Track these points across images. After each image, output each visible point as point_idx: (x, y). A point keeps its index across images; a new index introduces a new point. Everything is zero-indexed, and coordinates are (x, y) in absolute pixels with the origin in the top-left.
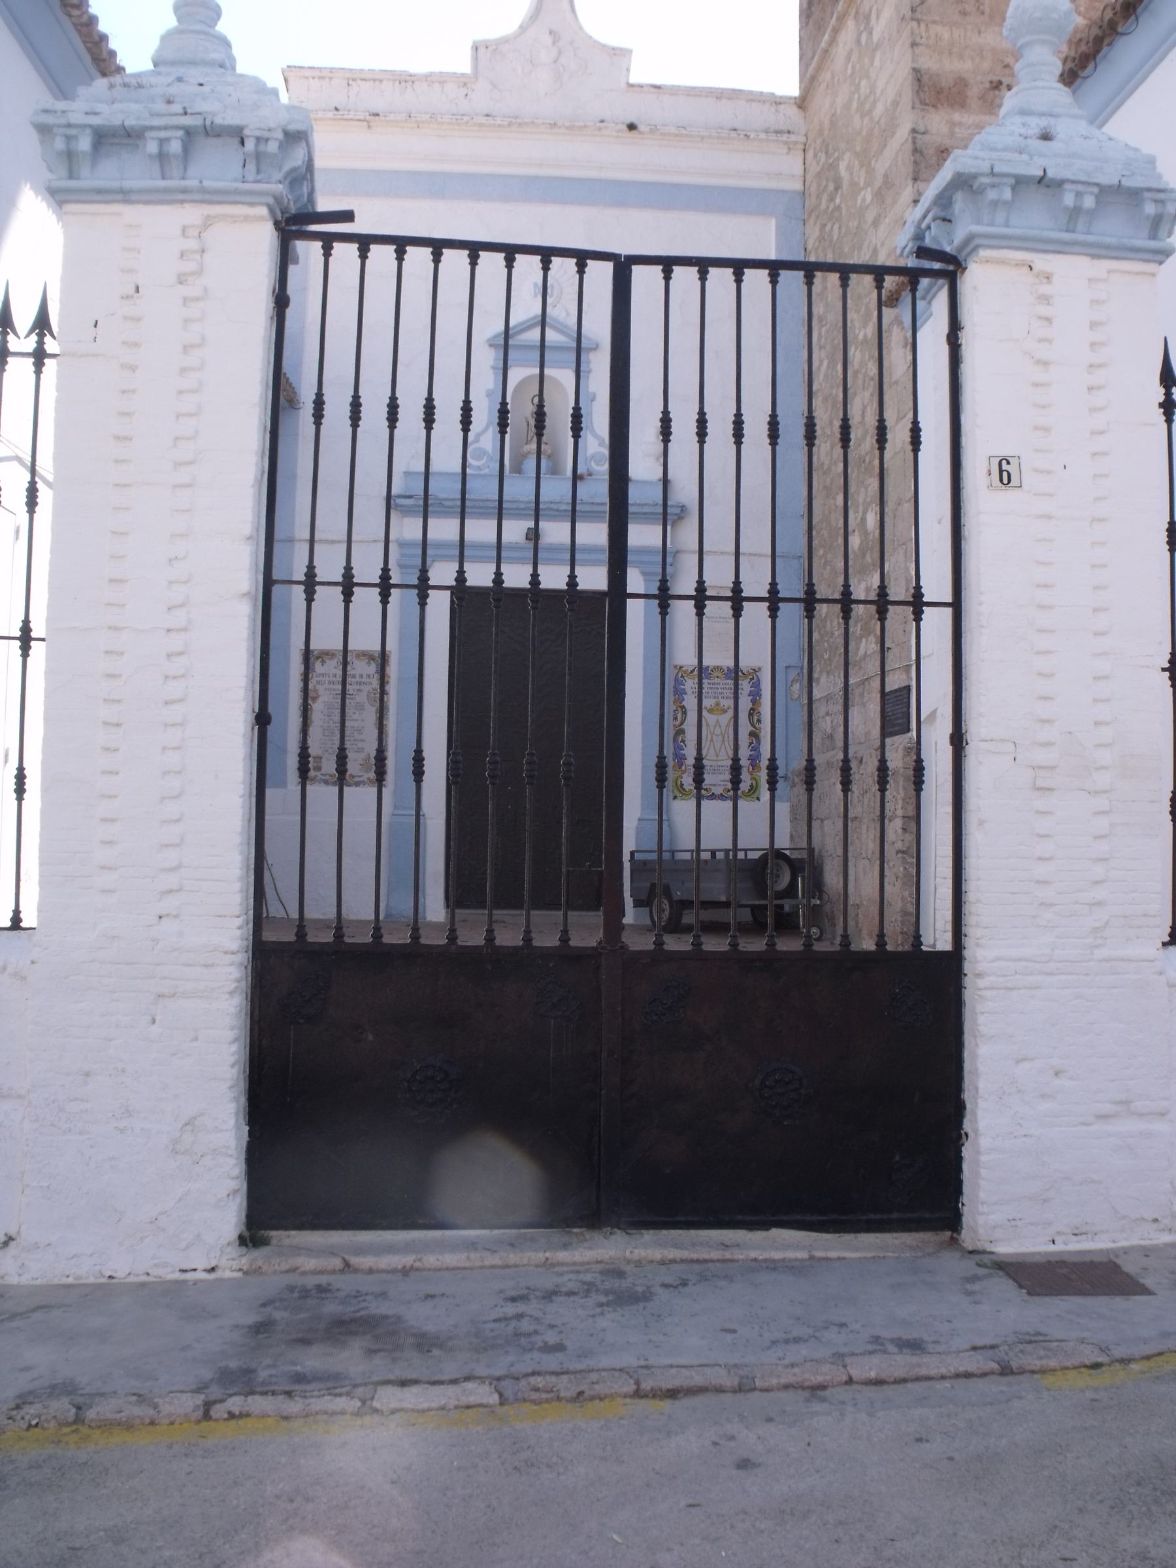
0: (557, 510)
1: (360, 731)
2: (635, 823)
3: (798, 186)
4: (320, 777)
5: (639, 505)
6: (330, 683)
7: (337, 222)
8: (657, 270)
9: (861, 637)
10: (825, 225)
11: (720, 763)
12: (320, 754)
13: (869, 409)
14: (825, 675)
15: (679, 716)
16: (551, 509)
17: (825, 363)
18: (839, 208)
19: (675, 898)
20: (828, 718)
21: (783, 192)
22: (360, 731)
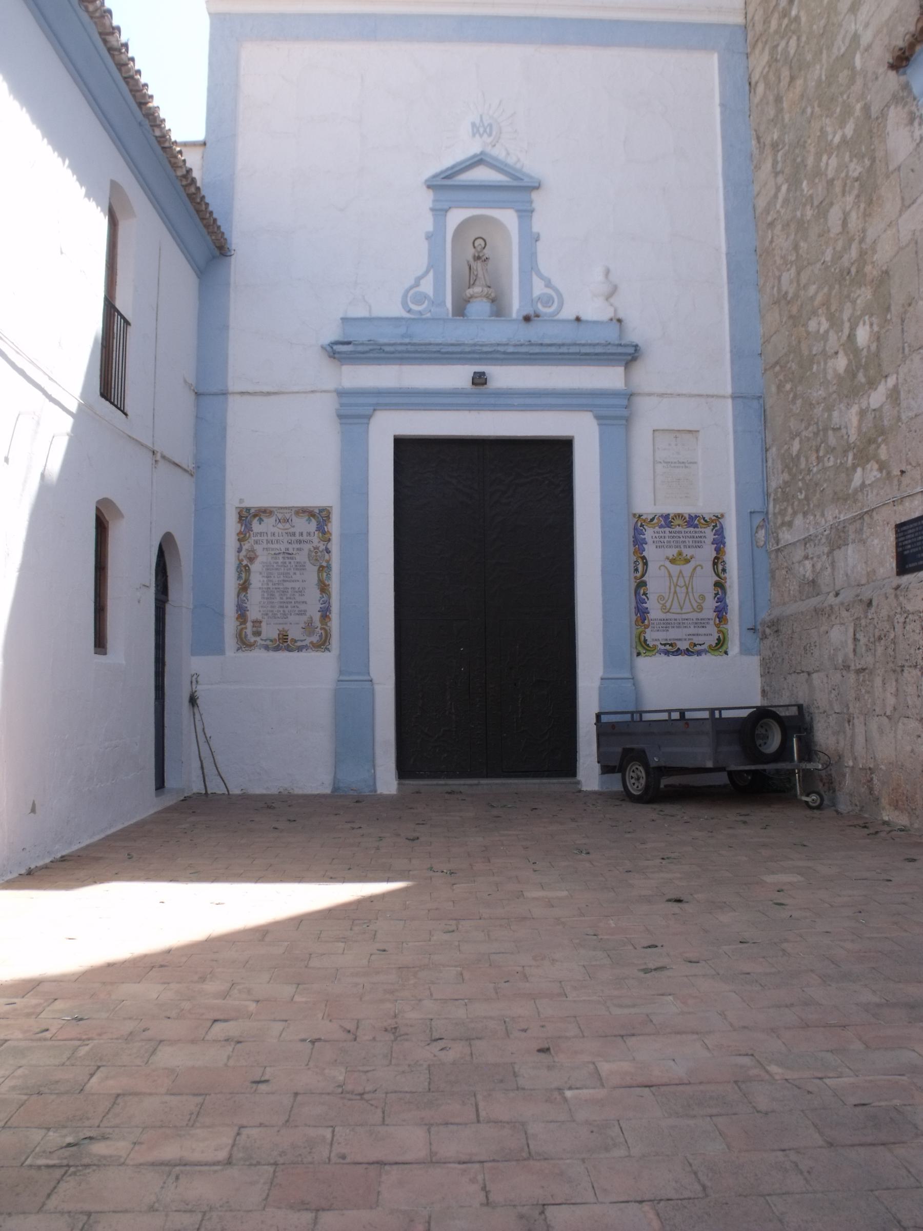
0: (505, 353)
2: (597, 683)
3: (740, 20)
5: (590, 345)
9: (854, 467)
10: (777, 46)
11: (684, 616)
12: (260, 618)
13: (854, 215)
14: (800, 516)
15: (640, 567)
16: (498, 352)
17: (784, 188)
18: (797, 19)
19: (653, 765)
20: (807, 562)
21: (725, 26)
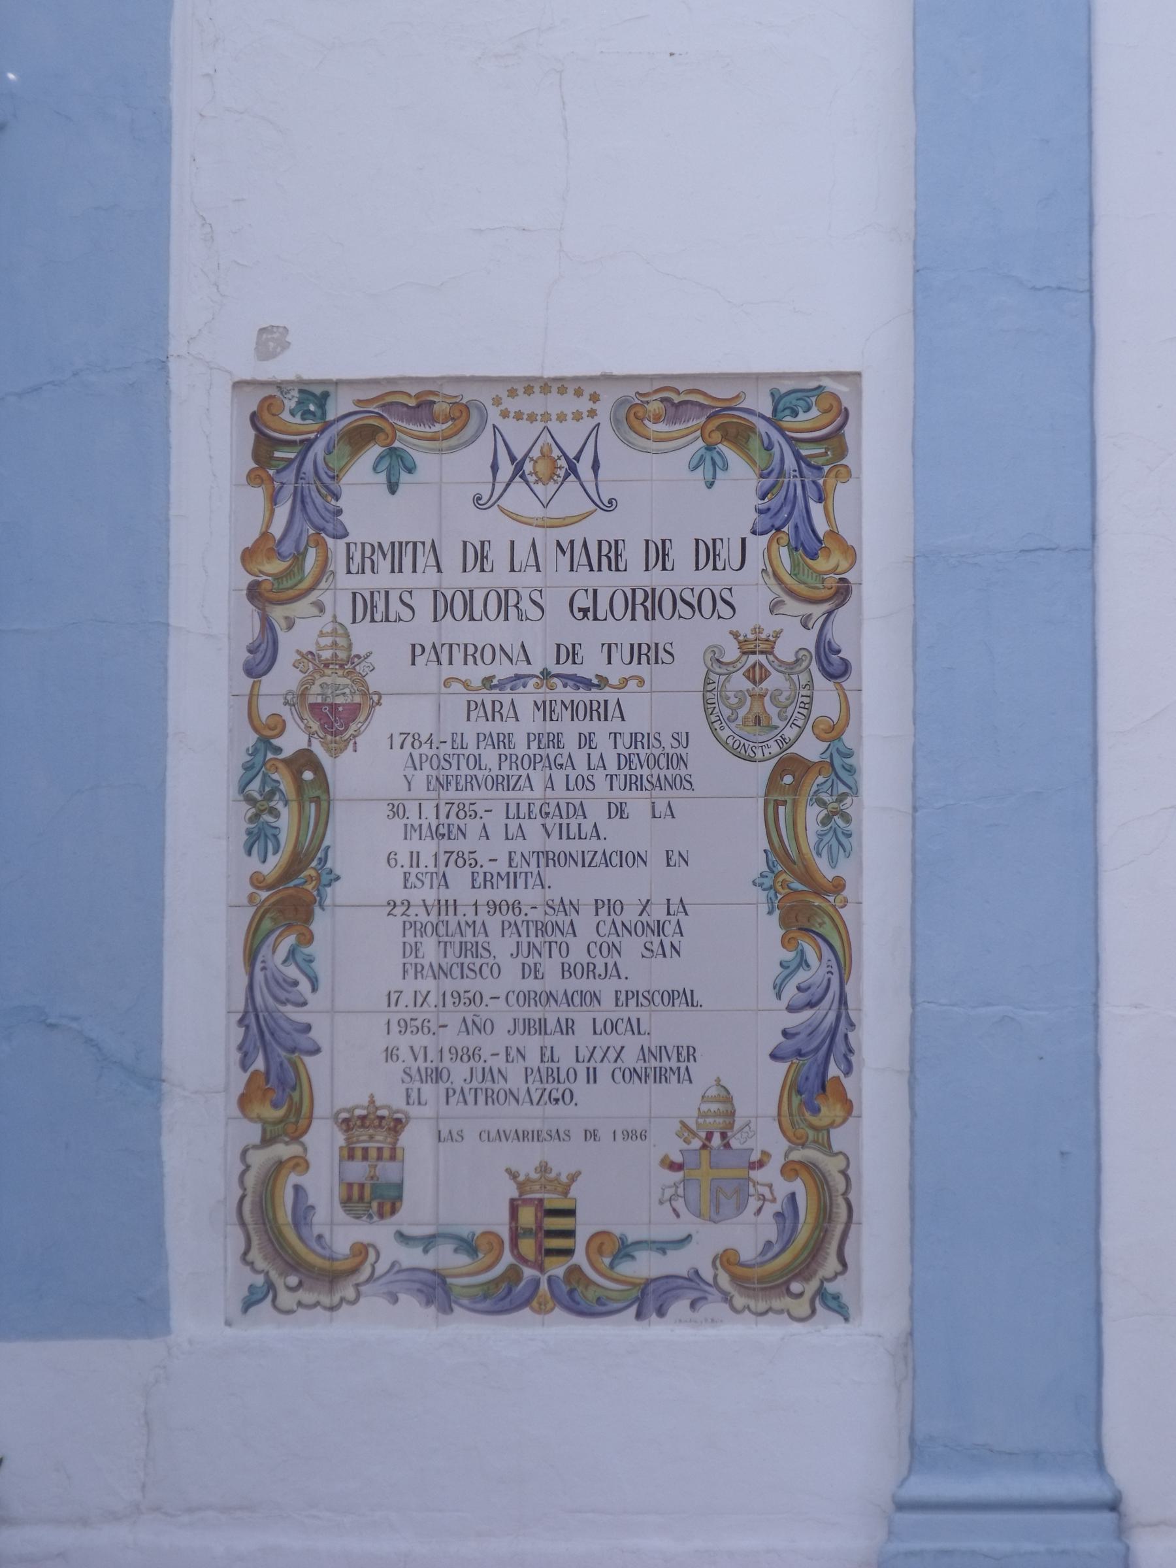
1: (660, 931)
4: (391, 1252)
6: (443, 605)
12: (391, 1097)
22: (660, 931)
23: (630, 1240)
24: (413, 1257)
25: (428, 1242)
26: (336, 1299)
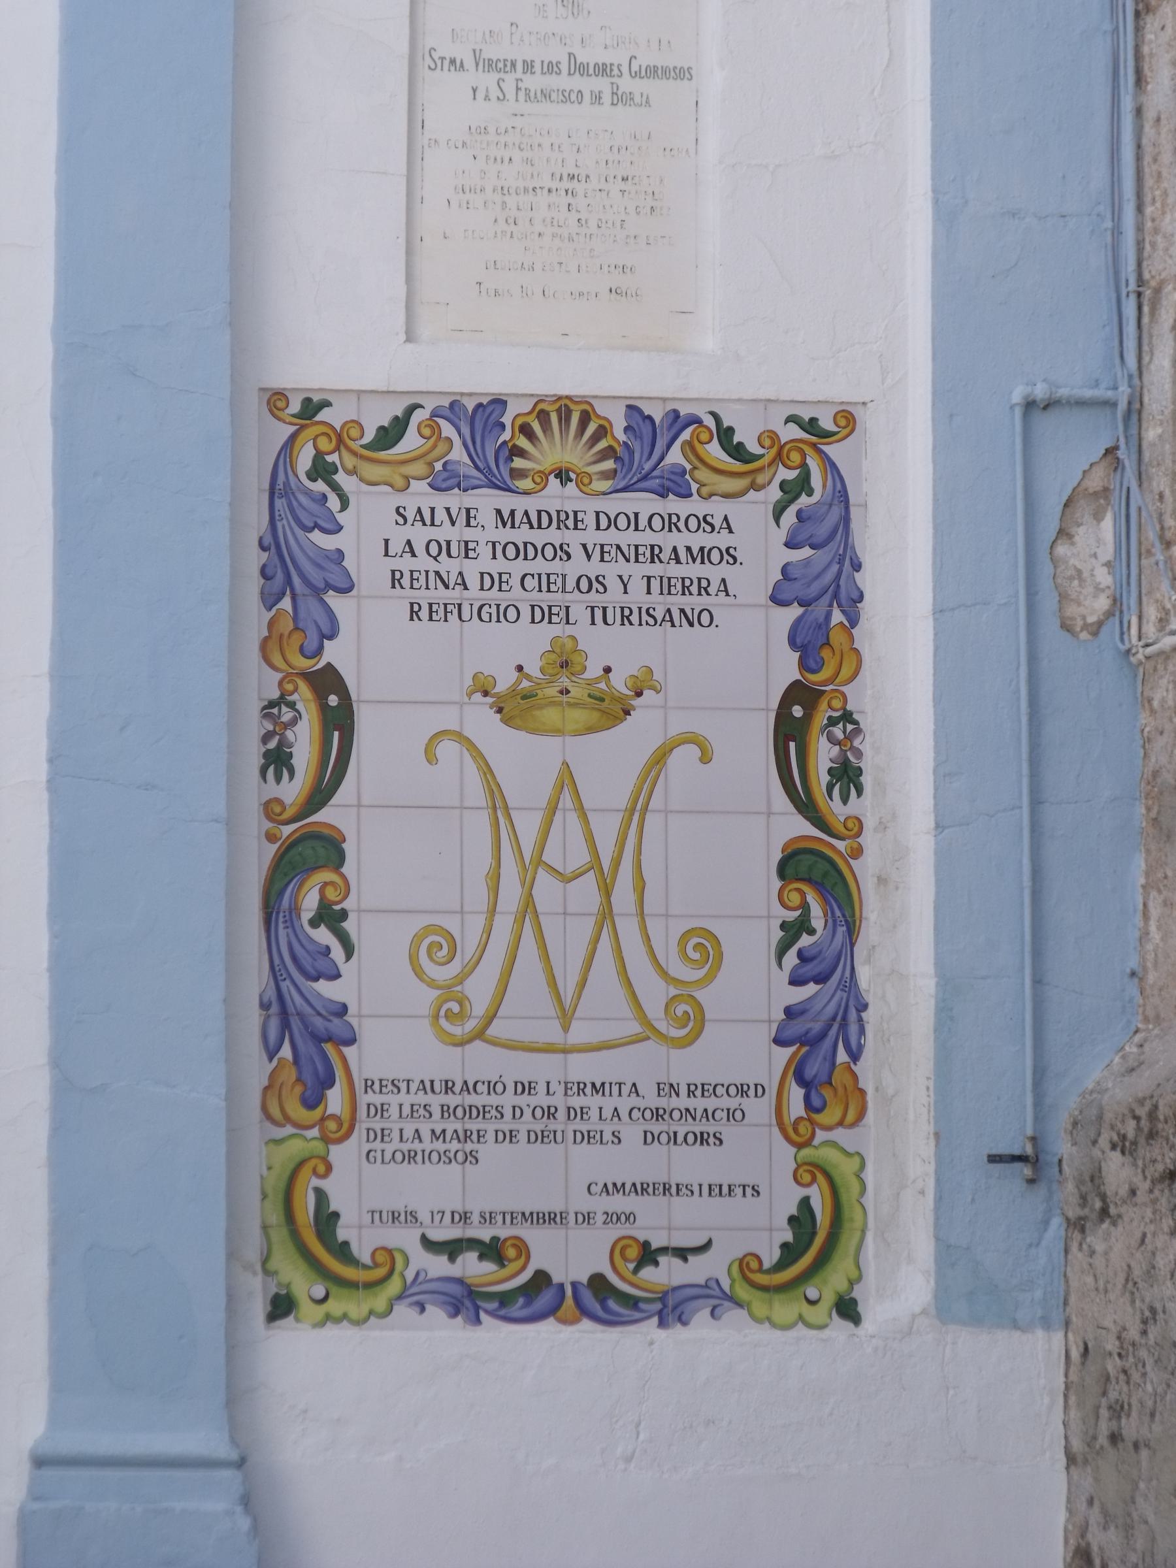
7: (1032, 838)
8: (354, 397)
11: (582, 1068)
23: (654, 1246)
24: (439, 1266)
25: (452, 1249)
26: (365, 1310)
